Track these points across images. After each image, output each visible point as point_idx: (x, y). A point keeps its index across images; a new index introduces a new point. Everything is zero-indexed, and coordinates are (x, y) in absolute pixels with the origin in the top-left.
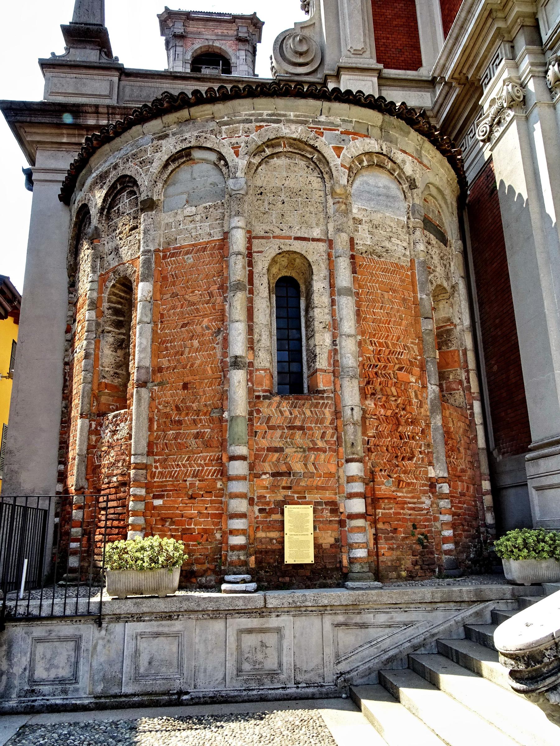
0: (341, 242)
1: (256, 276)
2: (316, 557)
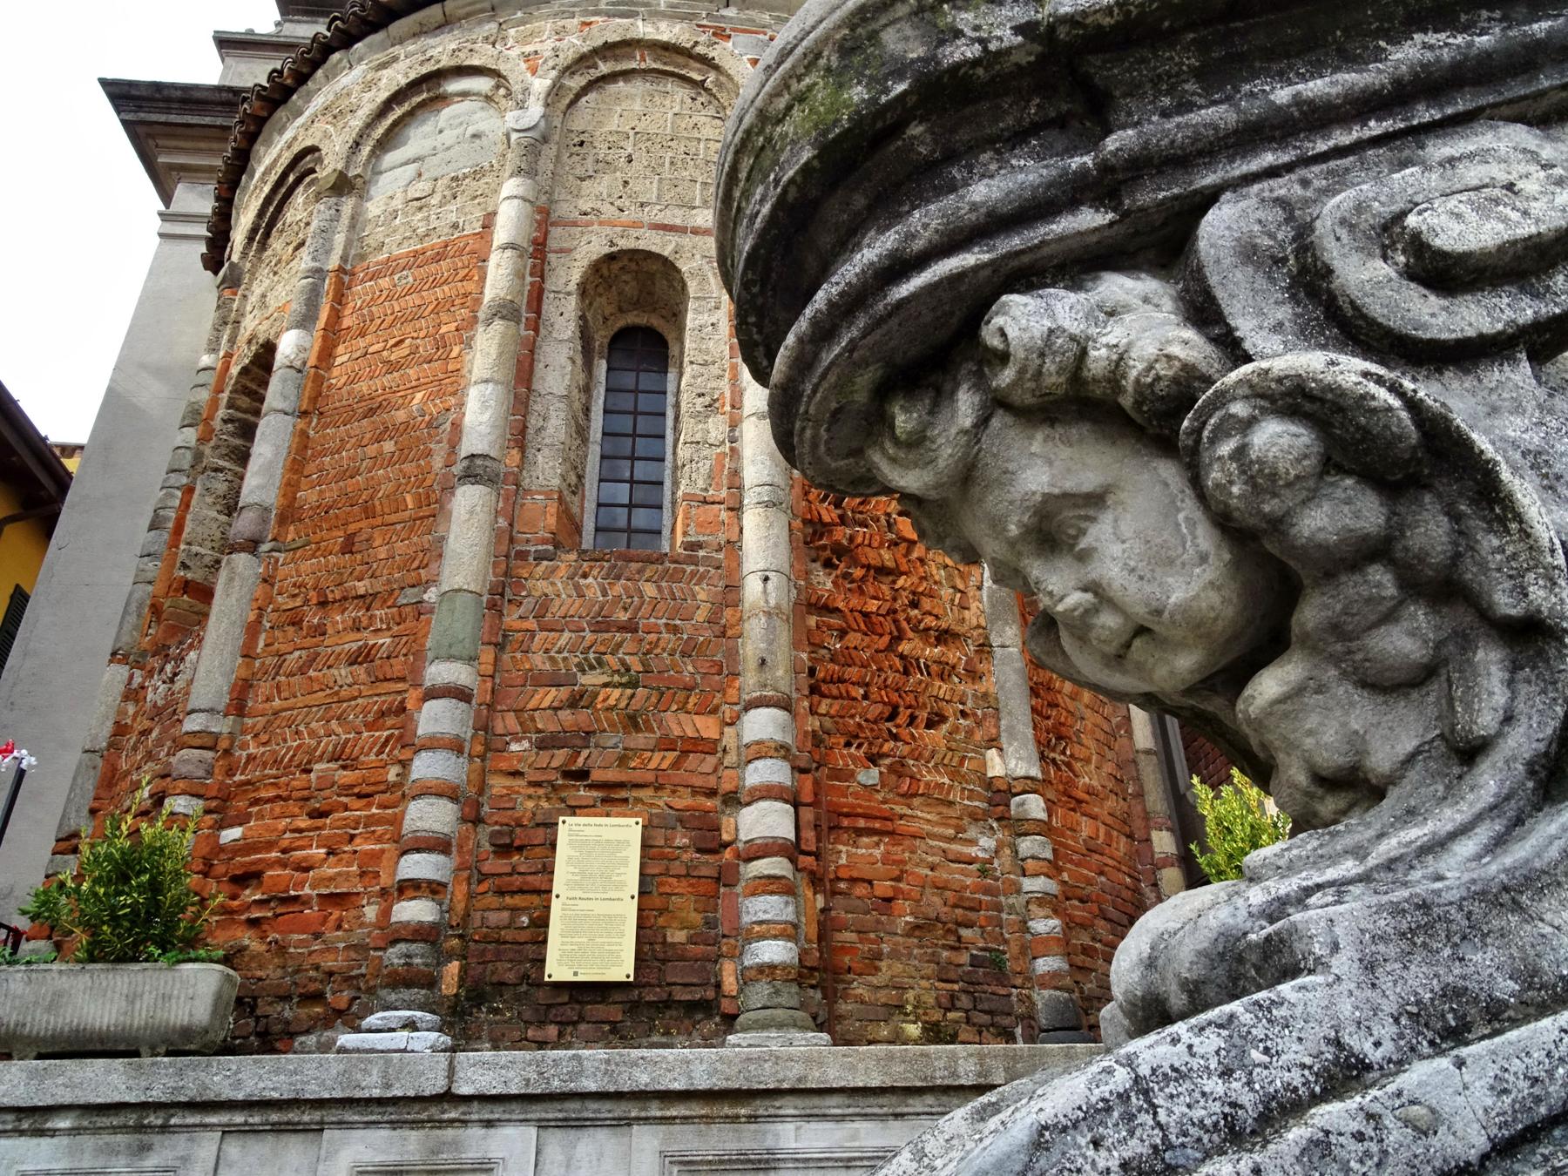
1: (548, 297)
2: (636, 969)
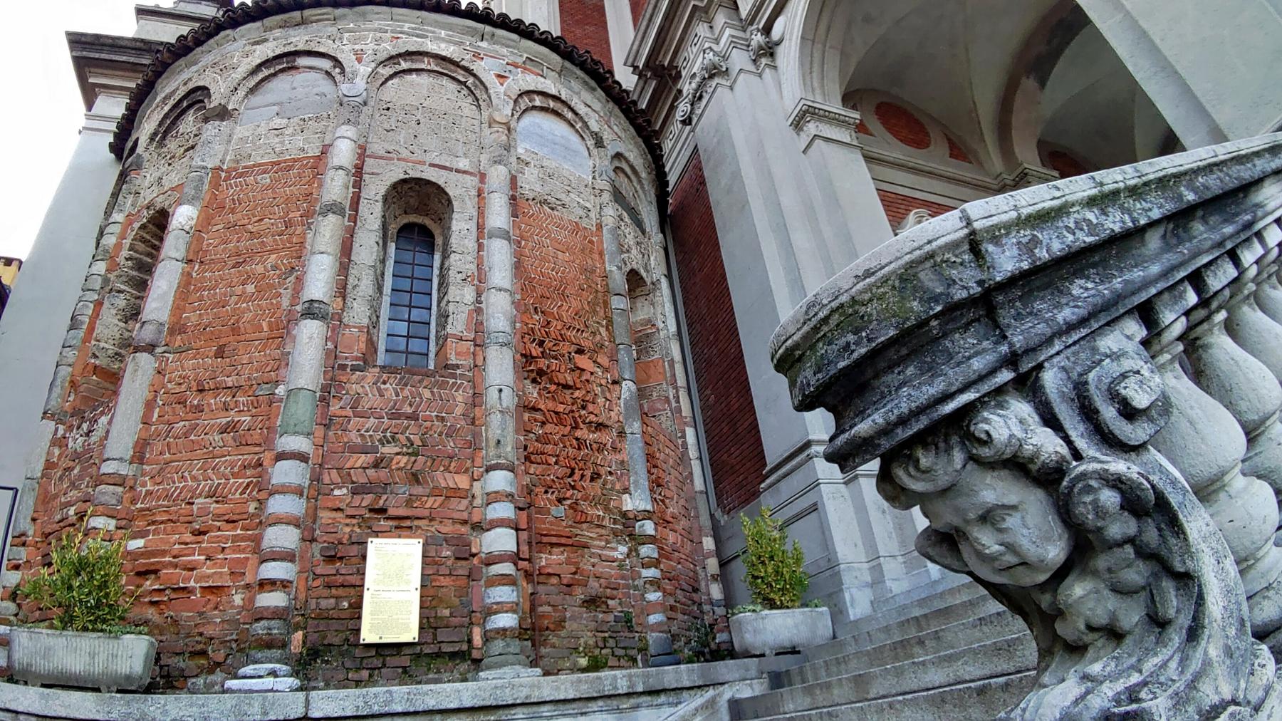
0: (498, 176)
